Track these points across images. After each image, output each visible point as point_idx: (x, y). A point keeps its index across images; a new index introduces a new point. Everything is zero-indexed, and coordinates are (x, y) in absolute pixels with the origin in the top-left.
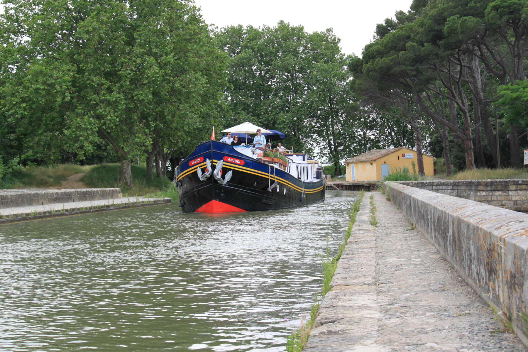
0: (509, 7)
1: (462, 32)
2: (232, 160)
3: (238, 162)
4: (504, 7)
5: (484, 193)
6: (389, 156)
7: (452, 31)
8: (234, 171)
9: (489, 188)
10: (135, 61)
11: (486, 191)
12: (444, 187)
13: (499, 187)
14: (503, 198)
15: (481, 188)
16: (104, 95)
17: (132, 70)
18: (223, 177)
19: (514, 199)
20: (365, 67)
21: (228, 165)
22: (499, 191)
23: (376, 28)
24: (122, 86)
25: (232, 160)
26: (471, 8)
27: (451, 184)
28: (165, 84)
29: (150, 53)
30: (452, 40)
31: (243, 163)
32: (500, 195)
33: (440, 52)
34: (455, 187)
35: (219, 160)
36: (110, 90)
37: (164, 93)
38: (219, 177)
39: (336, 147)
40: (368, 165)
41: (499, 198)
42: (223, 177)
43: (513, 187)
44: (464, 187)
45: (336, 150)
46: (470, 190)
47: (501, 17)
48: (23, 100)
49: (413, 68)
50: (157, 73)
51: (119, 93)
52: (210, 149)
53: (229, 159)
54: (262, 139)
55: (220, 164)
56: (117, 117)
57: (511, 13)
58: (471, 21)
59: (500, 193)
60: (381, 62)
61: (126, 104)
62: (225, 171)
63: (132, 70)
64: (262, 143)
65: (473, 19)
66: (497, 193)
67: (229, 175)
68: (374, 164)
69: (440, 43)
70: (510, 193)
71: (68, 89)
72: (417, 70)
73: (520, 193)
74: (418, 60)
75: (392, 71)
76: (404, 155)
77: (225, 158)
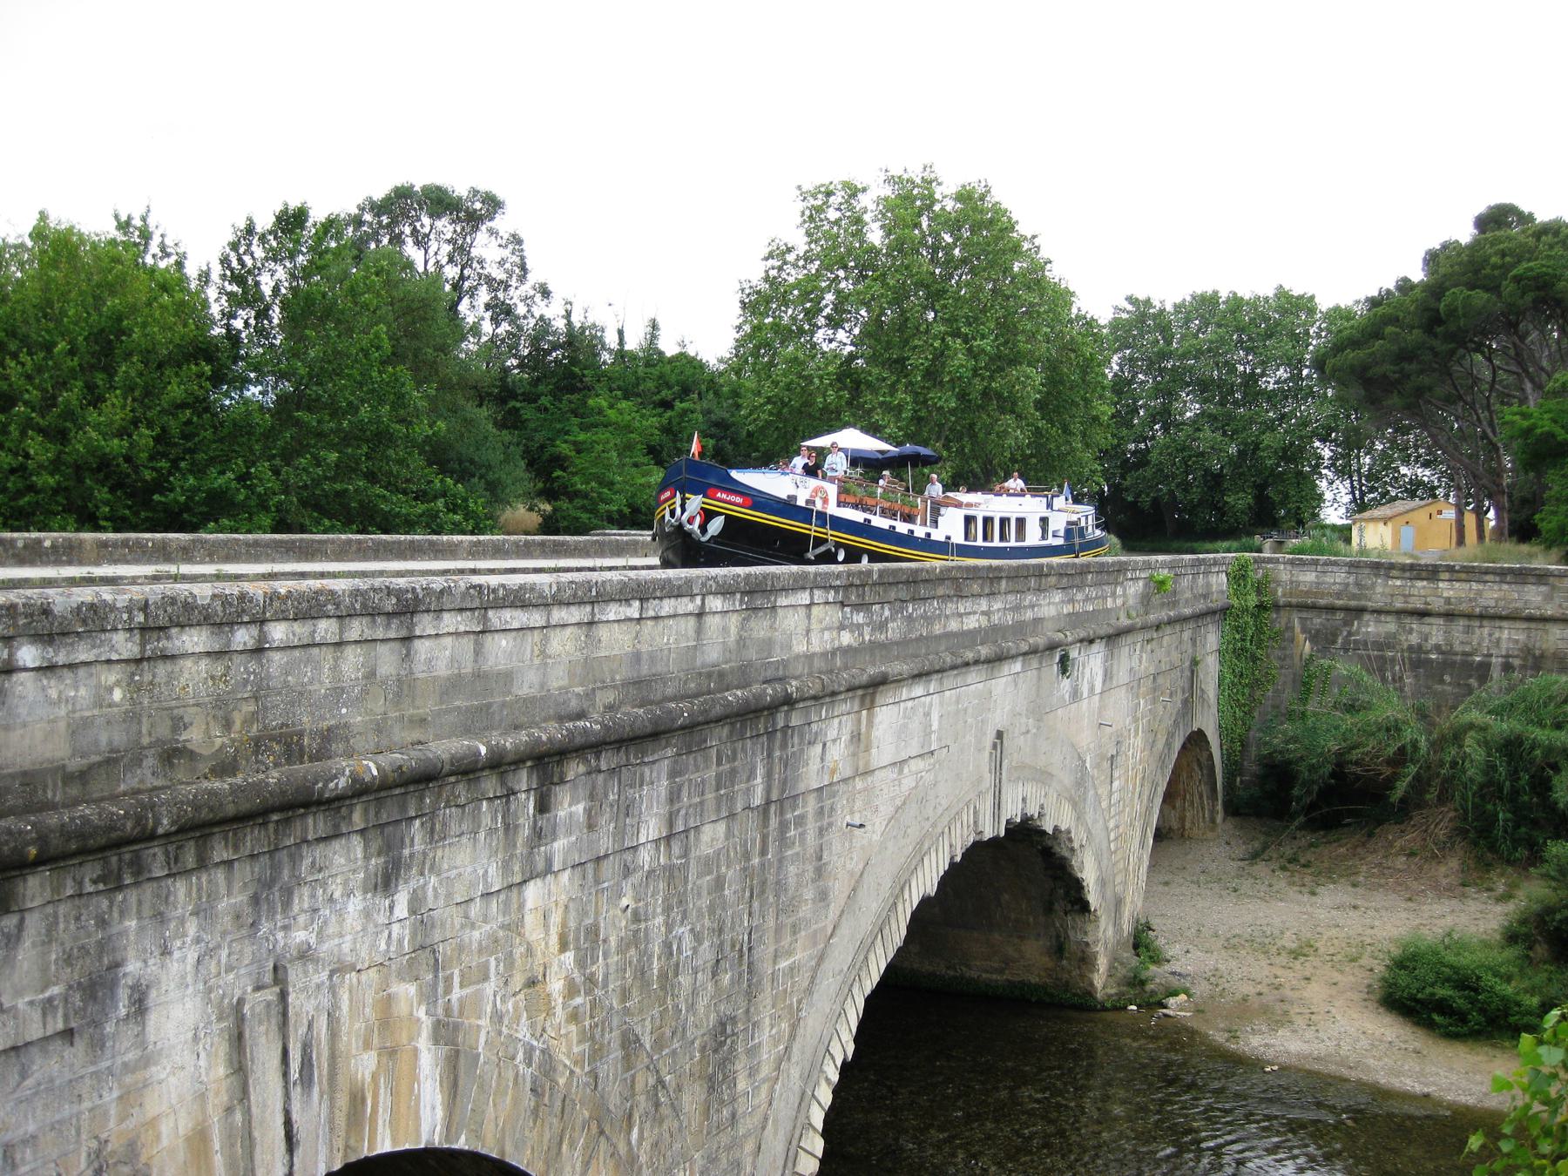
0: (1536, 278)
1: (1464, 315)
2: (724, 496)
3: (739, 500)
4: (1527, 278)
5: (1398, 583)
6: (1416, 513)
7: (1452, 312)
8: (727, 516)
9: (1408, 574)
10: (932, 345)
11: (1403, 578)
12: (1335, 569)
13: (1424, 574)
14: (1429, 592)
15: (1394, 573)
16: (883, 396)
17: (926, 359)
18: (703, 529)
19: (1445, 595)
20: (1330, 363)
21: (713, 505)
22: (1423, 579)
23: (1056, 273)
24: (911, 383)
25: (724, 496)
26: (1486, 276)
27: (1346, 564)
28: (976, 381)
29: (956, 334)
30: (1452, 327)
31: (749, 503)
32: (1424, 587)
33: (1436, 343)
34: (1353, 570)
35: (696, 493)
36: (893, 389)
37: (975, 395)
38: (695, 526)
39: (1363, 494)
40: (1381, 525)
41: (1422, 592)
42: (703, 529)
43: (1446, 576)
44: (1367, 571)
45: (1362, 499)
46: (1377, 576)
47: (1524, 293)
48: (769, 400)
49: (1397, 368)
50: (962, 366)
51: (906, 392)
52: (680, 474)
53: (719, 495)
54: (838, 460)
55: (695, 502)
56: (900, 429)
57: (1538, 288)
58: (1480, 297)
59: (1425, 583)
60: (1351, 355)
61: (916, 411)
62: (708, 515)
63: (926, 359)
64: (839, 467)
65: (1486, 296)
66: (1420, 584)
67: (716, 526)
68: (1390, 524)
69: (1439, 330)
70: (1441, 585)
71: (831, 385)
72: (1401, 371)
73: (1457, 585)
74: (1405, 356)
75: (1370, 373)
76: (1440, 512)
77: (710, 492)
